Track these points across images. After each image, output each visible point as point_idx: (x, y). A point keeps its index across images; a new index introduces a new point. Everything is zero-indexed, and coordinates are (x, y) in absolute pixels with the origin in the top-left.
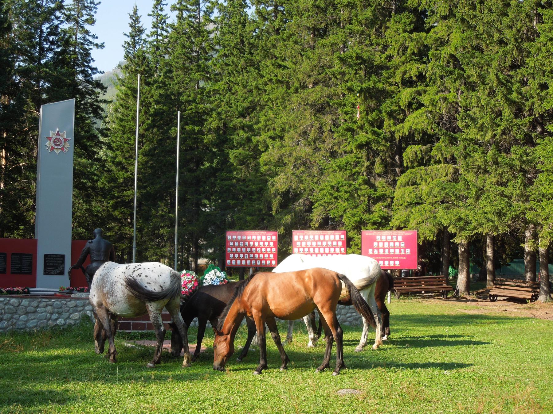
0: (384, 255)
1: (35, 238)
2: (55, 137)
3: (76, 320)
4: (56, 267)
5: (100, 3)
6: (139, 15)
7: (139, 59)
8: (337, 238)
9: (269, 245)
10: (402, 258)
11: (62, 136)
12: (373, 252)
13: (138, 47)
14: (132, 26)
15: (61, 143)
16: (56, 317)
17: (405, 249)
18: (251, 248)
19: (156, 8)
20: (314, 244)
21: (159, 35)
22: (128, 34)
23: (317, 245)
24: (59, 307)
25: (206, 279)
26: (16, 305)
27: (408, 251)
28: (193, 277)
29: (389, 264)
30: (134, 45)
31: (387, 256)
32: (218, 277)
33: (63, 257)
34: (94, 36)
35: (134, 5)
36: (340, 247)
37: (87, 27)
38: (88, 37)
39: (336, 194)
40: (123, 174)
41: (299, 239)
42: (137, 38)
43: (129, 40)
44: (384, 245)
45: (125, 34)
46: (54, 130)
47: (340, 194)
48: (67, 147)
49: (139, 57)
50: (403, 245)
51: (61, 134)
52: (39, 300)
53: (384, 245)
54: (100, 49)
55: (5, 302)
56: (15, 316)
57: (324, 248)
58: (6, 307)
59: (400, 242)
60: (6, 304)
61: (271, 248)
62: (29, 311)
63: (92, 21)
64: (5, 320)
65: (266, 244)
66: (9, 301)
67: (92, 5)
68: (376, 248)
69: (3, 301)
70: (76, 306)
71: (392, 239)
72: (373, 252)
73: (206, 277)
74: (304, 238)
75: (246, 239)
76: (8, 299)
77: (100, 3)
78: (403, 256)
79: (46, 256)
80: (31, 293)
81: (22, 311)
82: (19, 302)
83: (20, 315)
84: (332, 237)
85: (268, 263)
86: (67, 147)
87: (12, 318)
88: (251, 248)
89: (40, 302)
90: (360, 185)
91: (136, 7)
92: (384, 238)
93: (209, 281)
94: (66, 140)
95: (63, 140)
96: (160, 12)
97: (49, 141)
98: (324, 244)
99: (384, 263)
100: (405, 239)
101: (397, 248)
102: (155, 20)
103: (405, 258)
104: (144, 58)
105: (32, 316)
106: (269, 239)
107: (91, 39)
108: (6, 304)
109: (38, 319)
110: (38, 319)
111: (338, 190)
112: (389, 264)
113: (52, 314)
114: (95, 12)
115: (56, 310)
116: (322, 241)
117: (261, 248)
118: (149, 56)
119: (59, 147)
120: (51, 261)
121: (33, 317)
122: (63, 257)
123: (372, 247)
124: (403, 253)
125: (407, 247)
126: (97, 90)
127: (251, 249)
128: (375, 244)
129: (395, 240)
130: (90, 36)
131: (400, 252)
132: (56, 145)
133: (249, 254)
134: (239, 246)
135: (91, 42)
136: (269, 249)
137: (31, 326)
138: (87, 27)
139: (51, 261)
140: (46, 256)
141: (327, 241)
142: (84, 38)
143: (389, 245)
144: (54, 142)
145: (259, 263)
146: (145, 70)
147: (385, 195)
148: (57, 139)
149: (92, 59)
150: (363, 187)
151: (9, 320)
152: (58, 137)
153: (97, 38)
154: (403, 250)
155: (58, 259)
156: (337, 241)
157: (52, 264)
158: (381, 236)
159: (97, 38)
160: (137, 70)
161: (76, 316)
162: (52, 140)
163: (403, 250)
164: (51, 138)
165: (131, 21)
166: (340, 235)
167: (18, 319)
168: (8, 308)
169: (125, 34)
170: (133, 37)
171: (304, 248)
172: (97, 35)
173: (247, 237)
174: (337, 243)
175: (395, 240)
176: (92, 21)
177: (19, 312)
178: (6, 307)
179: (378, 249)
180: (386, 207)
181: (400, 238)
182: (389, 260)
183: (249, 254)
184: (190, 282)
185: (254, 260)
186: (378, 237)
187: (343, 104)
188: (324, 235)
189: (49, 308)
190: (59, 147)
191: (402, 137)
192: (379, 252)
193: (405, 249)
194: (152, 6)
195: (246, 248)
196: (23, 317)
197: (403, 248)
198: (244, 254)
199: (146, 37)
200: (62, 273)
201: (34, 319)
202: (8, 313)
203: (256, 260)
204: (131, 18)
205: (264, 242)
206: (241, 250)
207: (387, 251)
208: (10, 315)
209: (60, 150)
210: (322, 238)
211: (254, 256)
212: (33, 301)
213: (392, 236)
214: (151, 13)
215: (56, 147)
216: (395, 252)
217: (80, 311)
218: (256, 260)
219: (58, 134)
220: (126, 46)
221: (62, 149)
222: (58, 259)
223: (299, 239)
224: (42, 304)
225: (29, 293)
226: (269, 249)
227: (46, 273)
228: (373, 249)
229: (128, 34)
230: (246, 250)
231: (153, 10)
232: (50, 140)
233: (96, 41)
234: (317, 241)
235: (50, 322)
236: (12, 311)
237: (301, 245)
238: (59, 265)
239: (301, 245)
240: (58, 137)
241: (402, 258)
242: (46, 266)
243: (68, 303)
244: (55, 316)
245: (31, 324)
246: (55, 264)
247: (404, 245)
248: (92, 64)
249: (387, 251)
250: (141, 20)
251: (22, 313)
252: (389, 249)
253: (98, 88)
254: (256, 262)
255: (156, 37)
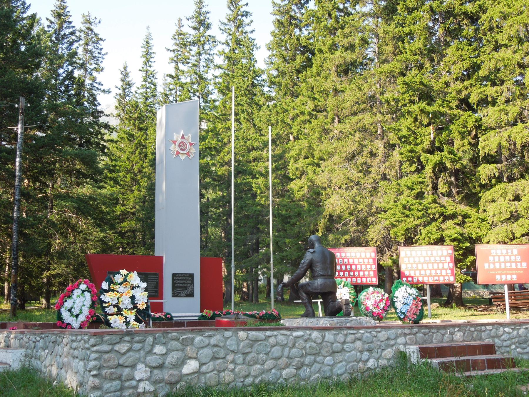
0: (501, 270)
1: (157, 254)
2: (180, 140)
3: (389, 360)
4: (186, 288)
5: (107, 53)
6: (128, 71)
7: (133, 107)
8: (445, 253)
9: (368, 262)
10: (519, 272)
11: (187, 139)
12: (489, 266)
13: (127, 98)
14: (123, 81)
15: (186, 148)
16: (367, 357)
17: (521, 263)
18: (351, 265)
19: (146, 64)
20: (422, 260)
21: (148, 88)
22: (119, 87)
23: (425, 260)
24: (370, 341)
25: (397, 298)
26: (319, 341)
27: (524, 265)
28: (383, 296)
29: (506, 279)
30: (125, 95)
31: (503, 270)
32: (410, 294)
33: (192, 276)
34: (100, 84)
35: (124, 63)
36: (449, 263)
37: (95, 74)
38: (95, 84)
39: (407, 213)
40: (120, 208)
41: (406, 255)
42: (127, 91)
43: (121, 92)
44: (499, 260)
45: (117, 87)
46: (179, 133)
47: (412, 212)
48: (192, 152)
49: (132, 105)
50: (519, 258)
51: (185, 137)
52: (345, 332)
53: (499, 260)
54: (106, 95)
55: (305, 338)
56: (318, 359)
57: (433, 263)
58: (308, 346)
59: (515, 255)
60: (306, 341)
61: (371, 265)
62: (336, 350)
63: (99, 69)
64: (307, 365)
65: (366, 260)
66: (310, 335)
67: (100, 56)
68: (491, 263)
69: (303, 336)
70: (388, 339)
71: (507, 253)
72: (489, 266)
73: (396, 295)
74: (411, 254)
75: (346, 256)
76: (308, 332)
77: (107, 53)
78: (519, 269)
79: (174, 275)
80: (175, 319)
81: (327, 350)
82: (322, 336)
83: (325, 357)
84: (440, 253)
85: (368, 281)
86: (192, 152)
87: (315, 361)
88: (351, 265)
89: (346, 335)
90: (430, 203)
91: (126, 64)
92: (499, 252)
93: (401, 299)
94: (191, 144)
95: (188, 144)
96: (149, 68)
97: (173, 145)
98: (432, 259)
99: (501, 277)
100: (520, 252)
101: (513, 262)
102: (144, 75)
103: (522, 272)
104: (137, 107)
105: (339, 357)
106: (368, 256)
107: (97, 85)
108: (306, 341)
109: (345, 361)
110: (345, 361)
111: (410, 210)
112: (506, 279)
113: (361, 352)
114: (101, 62)
115: (366, 346)
116: (430, 257)
117: (361, 265)
118: (141, 106)
119: (185, 152)
120: (180, 282)
121: (340, 358)
122: (192, 276)
123: (488, 261)
124: (519, 267)
125: (523, 260)
126: (103, 131)
127: (351, 267)
128: (491, 258)
129: (510, 254)
130: (96, 83)
131: (517, 265)
132: (182, 149)
133: (349, 272)
134: (507, 255)
135: (98, 89)
136: (369, 267)
137: (340, 372)
138: (95, 74)
139: (180, 282)
140: (174, 275)
141: (435, 257)
142: (91, 84)
143: (505, 260)
144: (179, 146)
145: (359, 281)
146: (138, 117)
147: (456, 213)
148: (182, 142)
149: (99, 104)
150: (433, 205)
151: (312, 366)
152: (183, 140)
153: (102, 85)
154: (519, 264)
155: (187, 278)
156: (445, 257)
157: (181, 285)
158: (496, 250)
159: (102, 85)
160: (130, 117)
161: (389, 353)
162: (177, 144)
163: (519, 264)
164: (176, 141)
165: (121, 76)
166: (447, 250)
167: (323, 363)
168: (310, 347)
169: (117, 87)
170: (124, 90)
171: (412, 264)
172: (102, 83)
173: (346, 254)
174: (445, 258)
175: (510, 254)
176: (99, 69)
177: (323, 352)
178: (308, 346)
179: (494, 263)
180: (458, 224)
181: (515, 252)
182: (506, 274)
183: (349, 272)
184: (381, 301)
185: (354, 277)
186: (493, 251)
187: (397, 129)
188: (432, 251)
189: (358, 344)
190: (185, 152)
191: (488, 154)
192: (495, 266)
193: (521, 263)
194: (142, 63)
195: (346, 265)
196: (328, 360)
197: (519, 262)
198: (344, 272)
199: (137, 89)
200: (191, 295)
201: (341, 362)
202: (310, 355)
203: (356, 278)
204: (122, 73)
205: (363, 259)
206: (341, 267)
207: (503, 265)
208: (313, 357)
209: (185, 156)
210: (429, 253)
211: (354, 273)
212: (338, 334)
213: (507, 250)
214: (141, 69)
215: (181, 152)
216: (511, 266)
217: (393, 346)
218: (356, 278)
219: (183, 137)
220: (118, 97)
221: (188, 154)
222: (187, 278)
223: (406, 255)
224: (350, 338)
225: (173, 320)
226: (369, 267)
227: (174, 295)
228: (489, 263)
229: (119, 87)
230: (346, 267)
231: (143, 66)
232: (175, 144)
233: (102, 88)
234: (425, 257)
235: (361, 364)
236: (315, 352)
237: (409, 261)
238: (188, 285)
239: (409, 261)
240: (183, 140)
241: (519, 272)
242: (174, 287)
243: (379, 335)
244: (366, 355)
245: (339, 369)
246: (183, 285)
247: (519, 259)
248: (99, 108)
249: (503, 265)
250: (130, 75)
251: (327, 354)
252: (505, 262)
253: (106, 129)
254: (357, 280)
255: (145, 90)
